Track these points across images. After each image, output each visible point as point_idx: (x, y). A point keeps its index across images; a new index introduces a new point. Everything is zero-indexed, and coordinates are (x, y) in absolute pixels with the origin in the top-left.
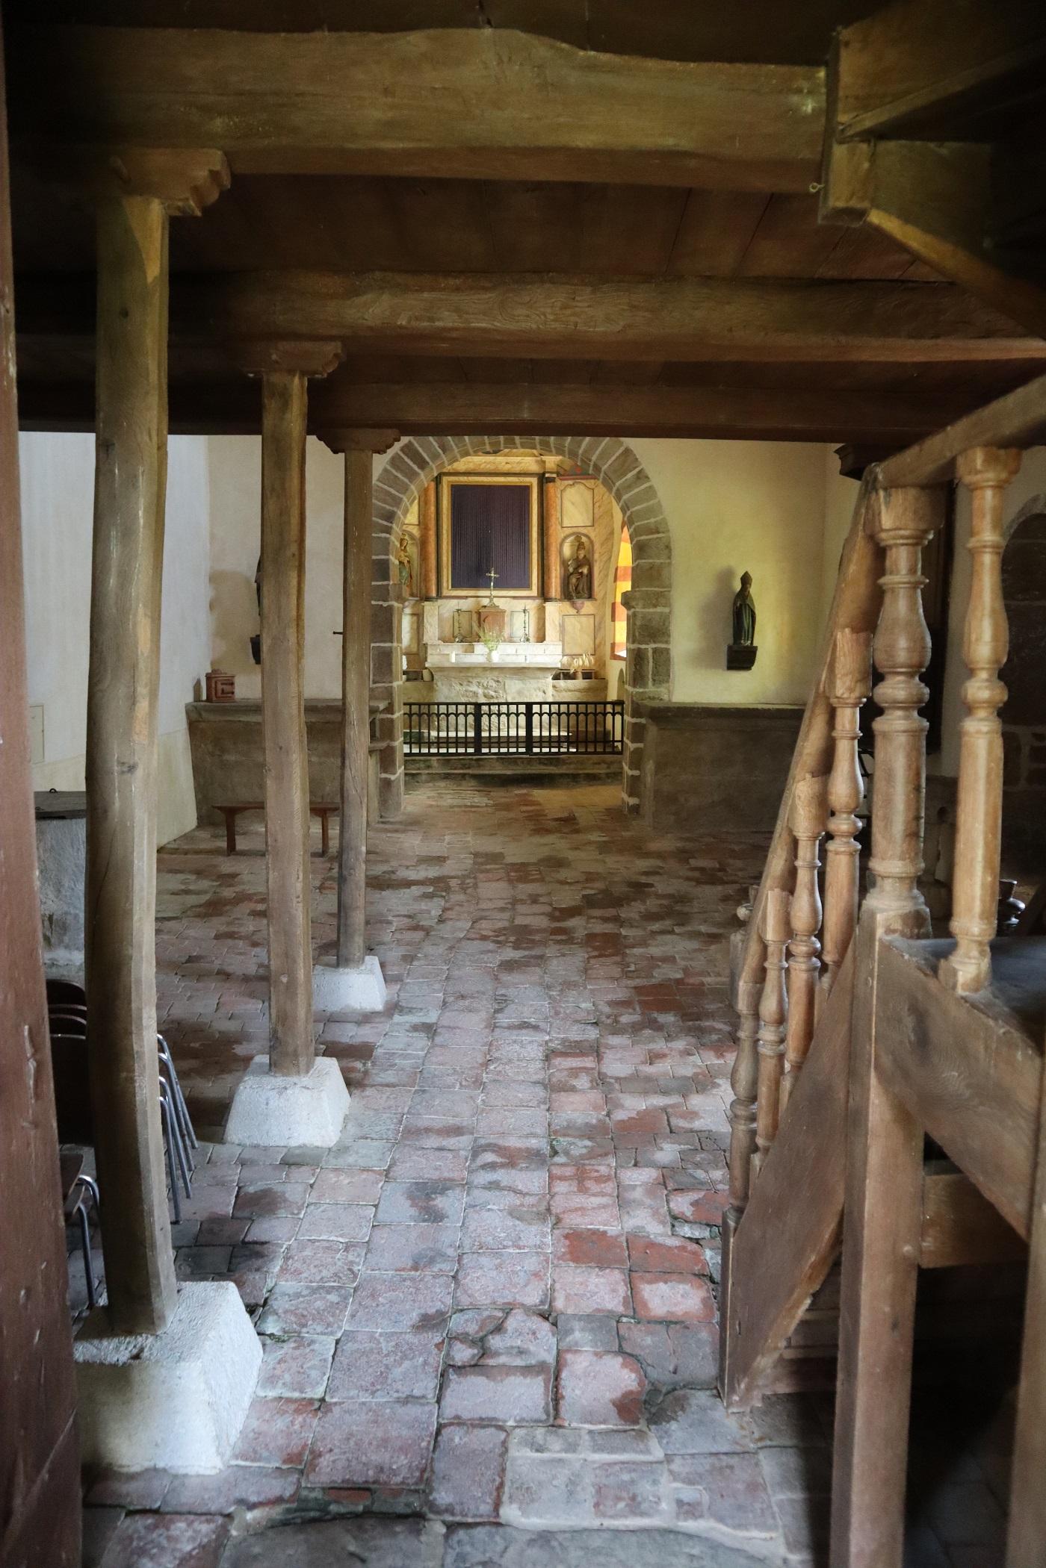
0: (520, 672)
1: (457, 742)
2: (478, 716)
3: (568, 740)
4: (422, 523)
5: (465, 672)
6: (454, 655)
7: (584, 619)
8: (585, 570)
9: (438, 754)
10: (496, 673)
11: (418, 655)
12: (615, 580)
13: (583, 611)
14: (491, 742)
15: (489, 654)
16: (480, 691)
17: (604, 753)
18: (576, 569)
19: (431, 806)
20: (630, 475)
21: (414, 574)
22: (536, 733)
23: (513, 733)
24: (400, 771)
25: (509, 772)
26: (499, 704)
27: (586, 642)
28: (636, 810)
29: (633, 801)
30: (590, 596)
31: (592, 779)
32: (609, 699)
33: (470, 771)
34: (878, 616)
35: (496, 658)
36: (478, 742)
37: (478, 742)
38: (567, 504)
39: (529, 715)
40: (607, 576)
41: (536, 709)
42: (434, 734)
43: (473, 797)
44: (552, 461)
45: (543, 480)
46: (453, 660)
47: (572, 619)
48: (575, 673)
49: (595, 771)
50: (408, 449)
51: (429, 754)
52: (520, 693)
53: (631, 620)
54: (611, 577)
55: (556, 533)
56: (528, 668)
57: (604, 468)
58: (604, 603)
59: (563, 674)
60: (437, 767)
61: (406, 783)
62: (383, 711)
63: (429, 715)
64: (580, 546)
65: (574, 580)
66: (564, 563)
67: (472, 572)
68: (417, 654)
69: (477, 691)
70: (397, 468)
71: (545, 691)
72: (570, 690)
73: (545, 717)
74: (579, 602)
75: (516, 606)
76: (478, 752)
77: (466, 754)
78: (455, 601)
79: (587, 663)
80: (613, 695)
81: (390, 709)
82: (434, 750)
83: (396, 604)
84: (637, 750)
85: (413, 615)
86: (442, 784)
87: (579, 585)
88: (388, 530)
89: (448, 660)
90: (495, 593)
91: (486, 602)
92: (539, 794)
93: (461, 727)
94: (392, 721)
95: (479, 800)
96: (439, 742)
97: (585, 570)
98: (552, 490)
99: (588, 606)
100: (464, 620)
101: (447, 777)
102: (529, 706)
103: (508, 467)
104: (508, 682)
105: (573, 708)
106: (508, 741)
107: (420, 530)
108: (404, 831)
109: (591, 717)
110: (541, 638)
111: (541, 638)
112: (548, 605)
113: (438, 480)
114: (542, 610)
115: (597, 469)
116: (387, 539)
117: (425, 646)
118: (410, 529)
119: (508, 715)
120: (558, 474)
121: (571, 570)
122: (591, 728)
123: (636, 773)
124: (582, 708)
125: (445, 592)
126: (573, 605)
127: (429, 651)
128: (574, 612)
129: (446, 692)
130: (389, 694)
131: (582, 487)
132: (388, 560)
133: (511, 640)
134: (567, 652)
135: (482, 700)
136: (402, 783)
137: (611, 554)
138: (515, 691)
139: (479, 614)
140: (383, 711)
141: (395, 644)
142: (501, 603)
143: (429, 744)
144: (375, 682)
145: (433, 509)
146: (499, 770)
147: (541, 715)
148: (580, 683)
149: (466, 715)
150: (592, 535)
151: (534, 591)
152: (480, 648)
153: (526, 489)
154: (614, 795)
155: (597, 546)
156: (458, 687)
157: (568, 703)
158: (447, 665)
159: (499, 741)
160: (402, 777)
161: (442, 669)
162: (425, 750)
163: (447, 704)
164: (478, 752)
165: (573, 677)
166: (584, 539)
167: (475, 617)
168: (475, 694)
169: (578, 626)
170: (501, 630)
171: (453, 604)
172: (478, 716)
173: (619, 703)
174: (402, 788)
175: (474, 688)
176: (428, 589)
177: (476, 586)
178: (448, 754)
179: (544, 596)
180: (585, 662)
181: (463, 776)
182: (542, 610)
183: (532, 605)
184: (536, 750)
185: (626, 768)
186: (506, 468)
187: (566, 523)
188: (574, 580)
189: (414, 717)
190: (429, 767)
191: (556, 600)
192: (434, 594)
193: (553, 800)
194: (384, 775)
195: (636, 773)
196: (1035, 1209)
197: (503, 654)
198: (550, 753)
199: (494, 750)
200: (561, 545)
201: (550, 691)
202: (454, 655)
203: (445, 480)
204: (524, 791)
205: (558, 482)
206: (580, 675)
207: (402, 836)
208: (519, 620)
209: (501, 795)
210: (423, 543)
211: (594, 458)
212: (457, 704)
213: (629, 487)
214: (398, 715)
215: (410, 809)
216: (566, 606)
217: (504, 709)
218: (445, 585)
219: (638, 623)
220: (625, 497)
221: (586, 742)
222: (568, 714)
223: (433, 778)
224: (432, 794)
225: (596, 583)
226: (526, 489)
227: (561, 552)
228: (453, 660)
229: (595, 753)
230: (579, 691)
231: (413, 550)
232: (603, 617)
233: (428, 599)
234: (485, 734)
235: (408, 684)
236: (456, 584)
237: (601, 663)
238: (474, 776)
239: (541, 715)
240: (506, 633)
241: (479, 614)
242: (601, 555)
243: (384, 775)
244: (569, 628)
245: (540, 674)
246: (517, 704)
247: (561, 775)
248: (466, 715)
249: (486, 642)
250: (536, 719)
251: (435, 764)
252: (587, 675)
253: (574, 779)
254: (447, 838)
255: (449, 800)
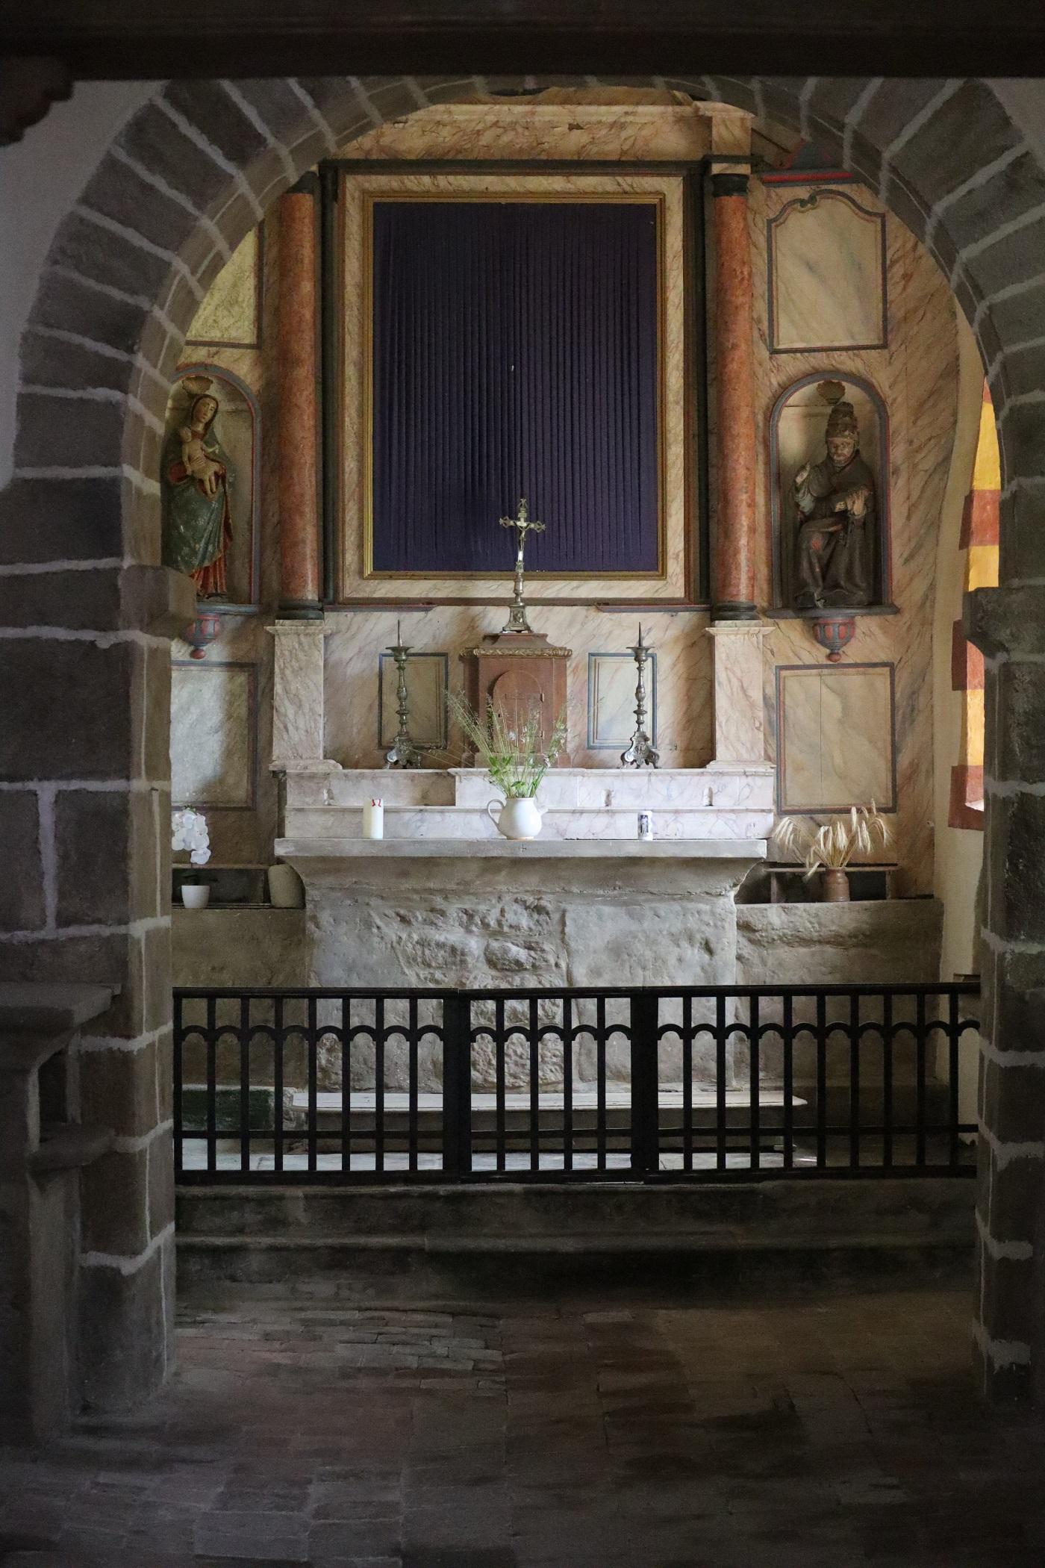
0: (622, 873)
1: (382, 1132)
2: (458, 1038)
3: (787, 1126)
4: (271, 340)
5: (420, 876)
6: (381, 812)
7: (855, 681)
8: (857, 506)
9: (312, 1176)
10: (532, 880)
11: (249, 807)
12: (965, 542)
13: (852, 653)
14: (504, 1129)
15: (508, 810)
16: (475, 945)
17: (920, 1170)
18: (824, 500)
19: (274, 1370)
20: (981, 177)
21: (239, 522)
22: (670, 1099)
23: (585, 1099)
24: (160, 1240)
25: (568, 1245)
26: (534, 996)
27: (865, 763)
28: (1016, 1382)
29: (1004, 1354)
30: (876, 597)
31: (874, 1267)
32: (947, 977)
33: (425, 1242)
34: (419, 858)
35: (532, 822)
36: (457, 1130)
37: (457, 1130)
38: (789, 269)
39: (645, 1033)
40: (934, 524)
41: (670, 1011)
42: (298, 1099)
43: (431, 1338)
44: (730, 121)
45: (705, 184)
46: (377, 830)
47: (812, 681)
48: (824, 876)
49: (889, 1240)
50: (144, 135)
51: (278, 1177)
52: (618, 950)
53: (998, 689)
54: (951, 530)
55: (753, 373)
56: (652, 862)
57: (890, 152)
58: (927, 623)
59: (774, 881)
60: (305, 1229)
61: (183, 1285)
62: (91, 1026)
63: (278, 1034)
64: (835, 415)
65: (816, 541)
66: (780, 479)
67: (444, 522)
68: (250, 808)
69: (464, 946)
70: (155, 159)
71: (709, 944)
72: (800, 943)
73: (704, 1042)
74: (836, 618)
75: (606, 635)
76: (457, 1167)
77: (413, 1176)
78: (386, 619)
79: (865, 839)
80: (959, 959)
81: (118, 1018)
82: (295, 1162)
83: (143, 640)
84: (1019, 1166)
85: (233, 666)
86: (322, 1287)
87: (831, 560)
88: (119, 376)
89: (360, 830)
90: (530, 588)
91: (498, 619)
92: (678, 1327)
93: (551, 1072)
94: (125, 1061)
95: (454, 1348)
96: (317, 1132)
97: (857, 506)
98: (735, 224)
99: (869, 636)
100: (420, 685)
101: (339, 1260)
102: (645, 1000)
103: (579, 138)
104: (575, 911)
105: (804, 1007)
106: (570, 1129)
107: (261, 362)
108: (161, 1464)
109: (871, 1041)
110: (699, 752)
111: (699, 752)
112: (728, 636)
113: (326, 183)
114: (700, 653)
115: (867, 153)
116: (113, 407)
117: (279, 778)
118: (225, 359)
119: (567, 1034)
120: (756, 161)
121: (806, 503)
122: (871, 1078)
123: (1019, 1250)
124: (871, 1010)
125: (352, 586)
126: (816, 630)
127: (292, 800)
128: (820, 654)
129: (357, 948)
130: (117, 959)
131: (843, 209)
132: (115, 483)
133: (588, 760)
134: (795, 798)
135: (483, 979)
136: (165, 1284)
137: (948, 451)
138: (598, 945)
139: (472, 663)
140: (91, 1026)
141: (139, 784)
142: (554, 626)
143: (281, 1143)
144: (63, 921)
145: (307, 288)
146: (534, 1237)
147: (687, 1033)
148: (838, 913)
149: (413, 1034)
150: (882, 379)
151: (674, 584)
152: (474, 789)
153: (645, 218)
154: (935, 1328)
155: (898, 417)
156: (393, 931)
157: (787, 992)
158: (354, 849)
159: (533, 1131)
160: (168, 1264)
161: (334, 865)
162: (262, 1162)
163: (346, 995)
164: (457, 1167)
165: (814, 890)
166: (852, 393)
167: (458, 674)
168: (456, 955)
169: (834, 704)
170: (552, 719)
171: (379, 629)
172: (458, 1038)
173: (969, 987)
174: (167, 1304)
175: (452, 934)
176: (289, 576)
177: (464, 561)
178: (346, 1176)
179: (710, 598)
180: (855, 835)
181: (400, 1259)
182: (700, 653)
183: (664, 631)
184: (670, 1161)
185: (984, 1231)
186: (572, 143)
187: (788, 336)
188: (816, 541)
189: (362, 1040)
190: (276, 1223)
191: (750, 612)
192: (310, 593)
193: (717, 1344)
194: (97, 1259)
195: (1019, 1250)
196: (712, 471)
197: (558, 809)
198: (721, 1173)
199: (518, 1163)
200: (771, 414)
201: (731, 942)
202: (381, 812)
203: (353, 185)
204: (620, 1315)
205: (758, 192)
206: (840, 882)
207: (151, 1482)
208: (618, 683)
209: (533, 1331)
210: (272, 413)
211: (853, 118)
212: (380, 995)
213: (980, 219)
214: (150, 1038)
215: (196, 1378)
216: (789, 636)
217: (362, 1013)
218: (350, 558)
219: (1021, 703)
220: (965, 254)
221: (855, 1133)
222: (787, 1031)
223: (290, 1264)
224: (283, 1324)
225: (897, 550)
226: (645, 218)
227: (768, 439)
228: (378, 832)
229: (886, 1171)
230: (836, 941)
231: (235, 435)
232: (923, 674)
233: (291, 610)
234: (482, 1102)
235: (213, 916)
236: (390, 559)
237: (918, 842)
238: (436, 1258)
239: (687, 1033)
240: (571, 736)
241: (472, 663)
242: (914, 449)
243: (97, 1259)
244: (799, 712)
245: (690, 882)
246: (601, 995)
247: (762, 1256)
248: (413, 1034)
249: (496, 767)
250: (669, 1047)
251: (298, 1212)
252: (866, 884)
253: (804, 1271)
254: (317, 1491)
255: (340, 1350)
